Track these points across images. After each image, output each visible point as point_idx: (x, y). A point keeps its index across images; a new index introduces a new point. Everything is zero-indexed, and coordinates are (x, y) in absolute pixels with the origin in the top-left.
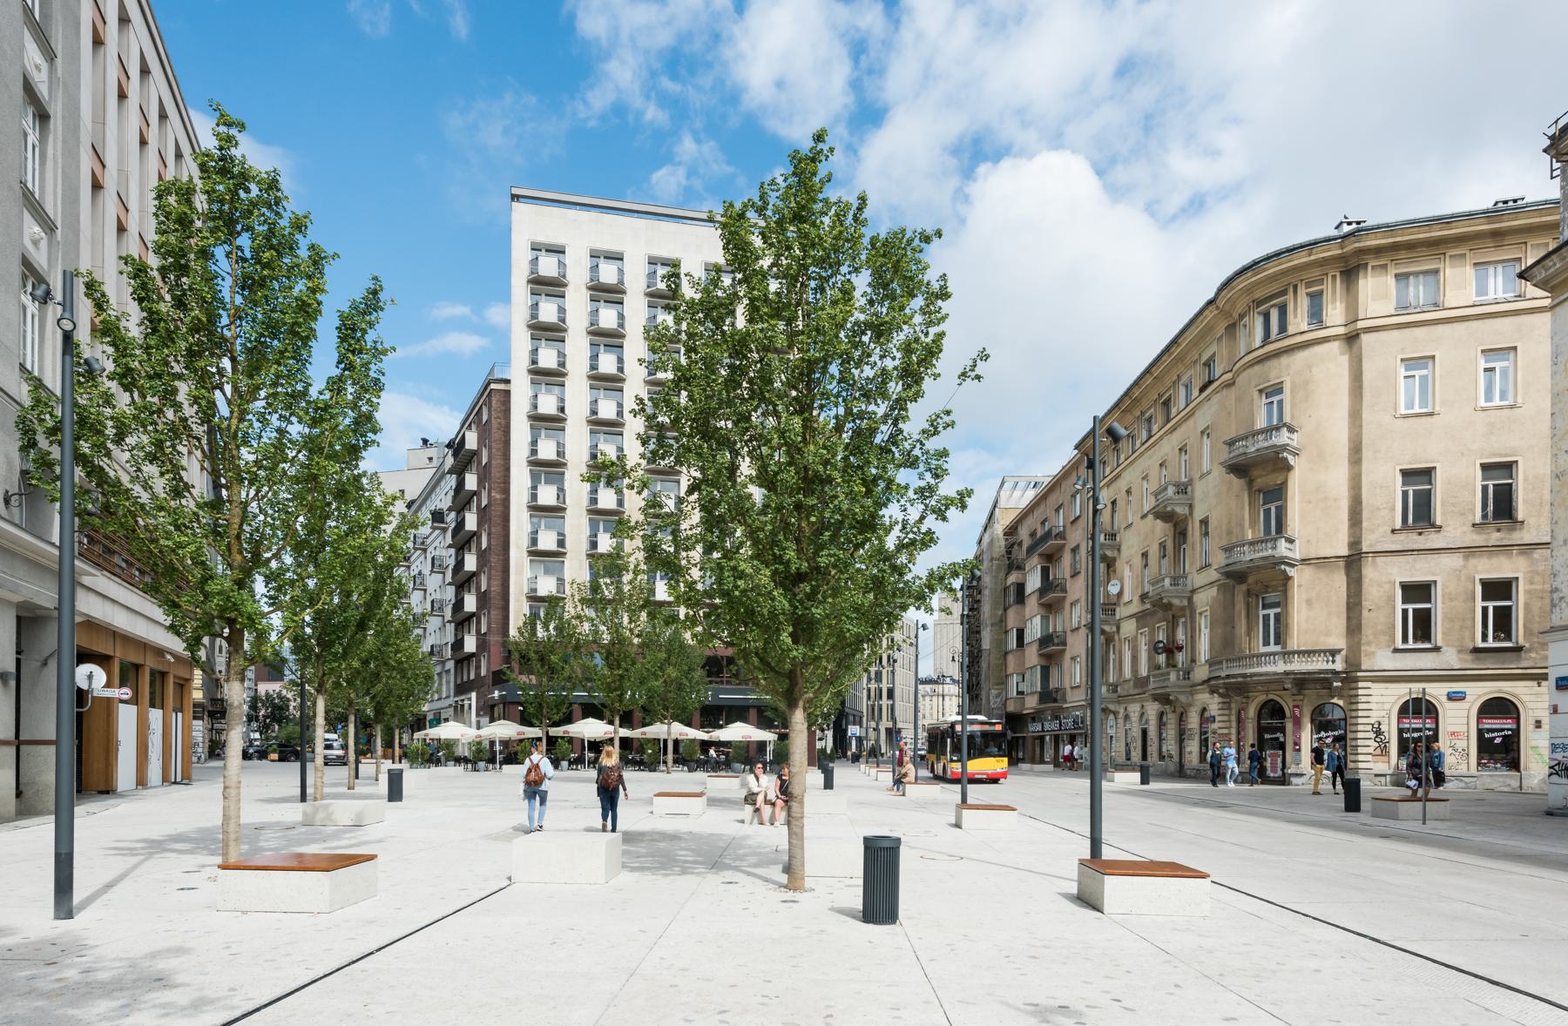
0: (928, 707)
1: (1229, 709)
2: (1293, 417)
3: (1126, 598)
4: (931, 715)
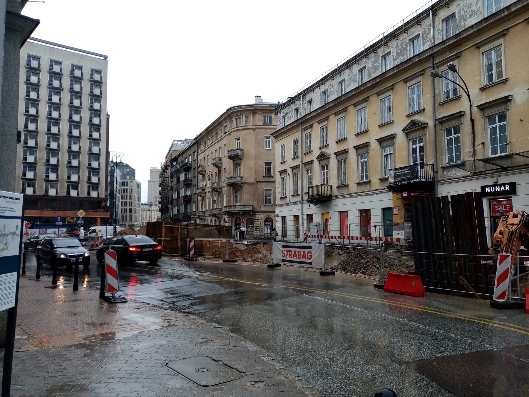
0: (145, 215)
1: (230, 219)
2: (242, 147)
3: (208, 186)
4: (146, 218)
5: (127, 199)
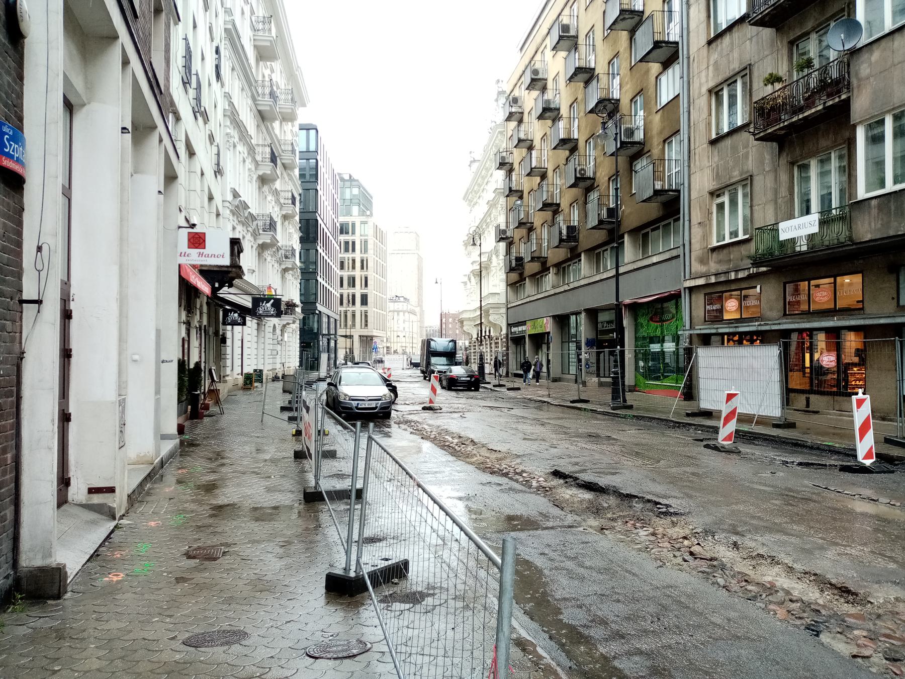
5: (354, 268)
